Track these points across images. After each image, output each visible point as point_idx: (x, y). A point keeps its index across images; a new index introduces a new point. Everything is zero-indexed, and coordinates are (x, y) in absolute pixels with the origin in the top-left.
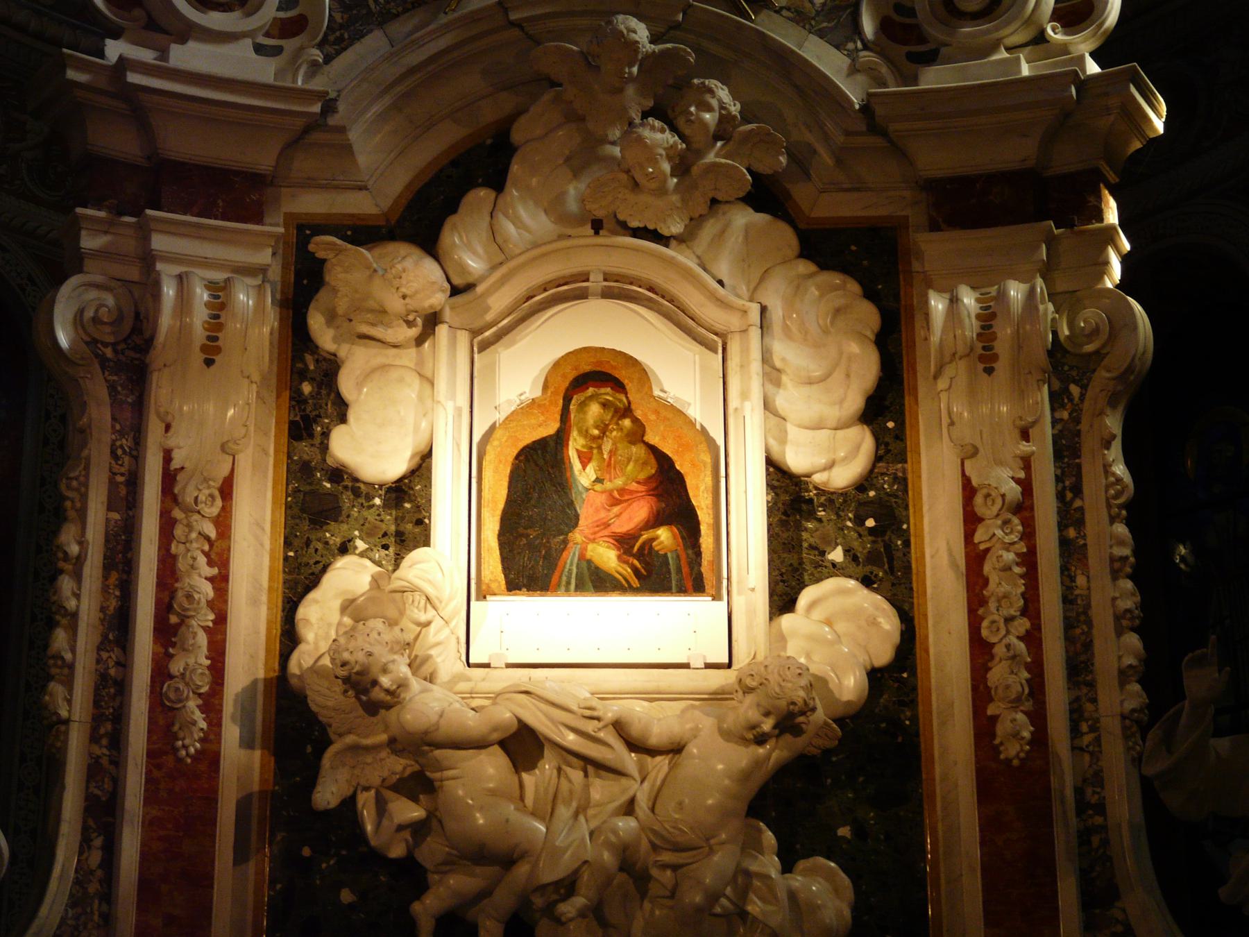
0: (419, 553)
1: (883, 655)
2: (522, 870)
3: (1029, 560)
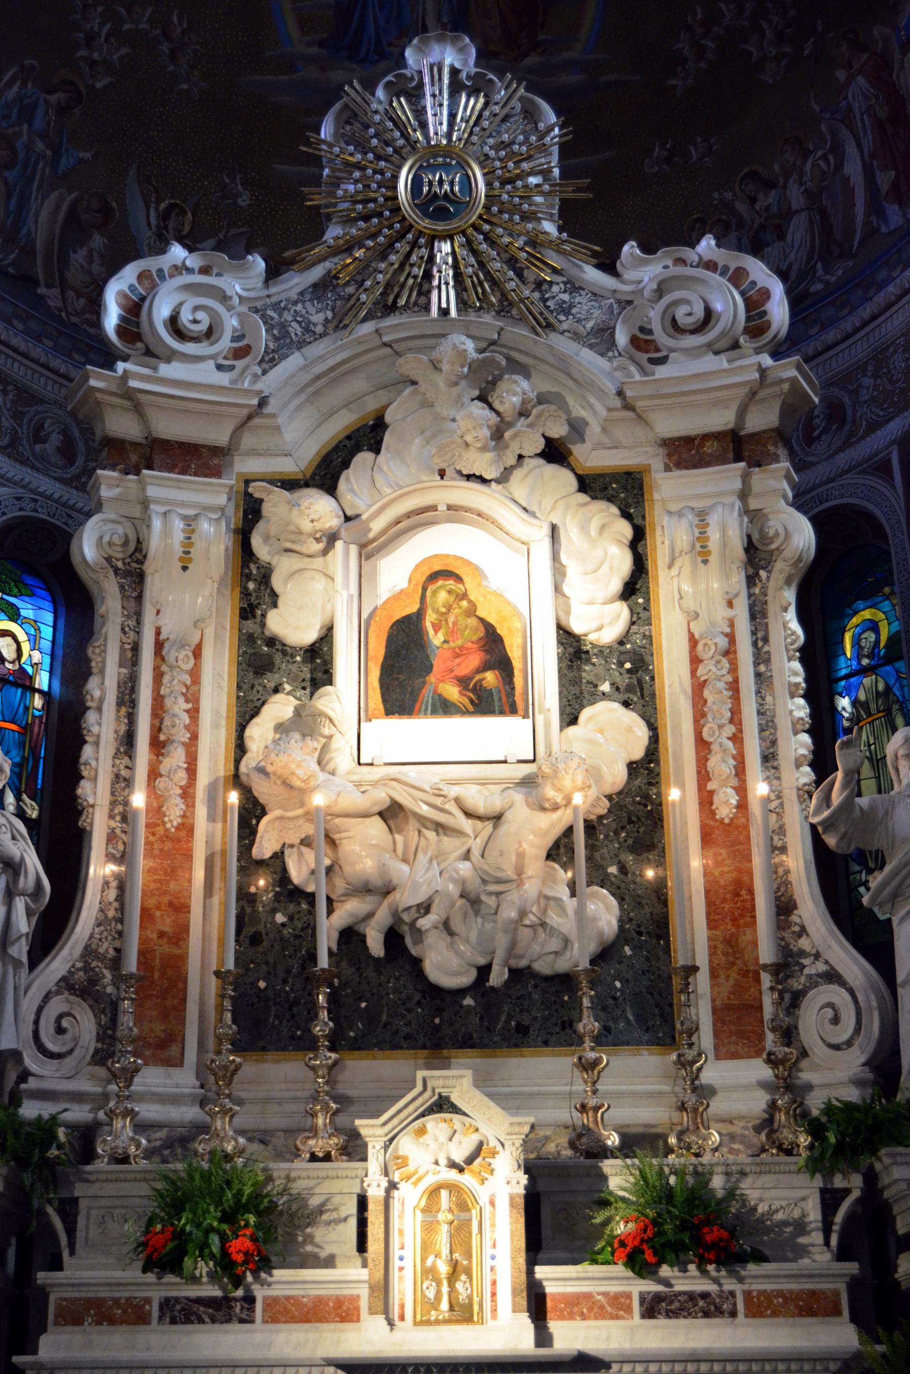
1: (638, 752)
2: (395, 896)
3: (734, 687)
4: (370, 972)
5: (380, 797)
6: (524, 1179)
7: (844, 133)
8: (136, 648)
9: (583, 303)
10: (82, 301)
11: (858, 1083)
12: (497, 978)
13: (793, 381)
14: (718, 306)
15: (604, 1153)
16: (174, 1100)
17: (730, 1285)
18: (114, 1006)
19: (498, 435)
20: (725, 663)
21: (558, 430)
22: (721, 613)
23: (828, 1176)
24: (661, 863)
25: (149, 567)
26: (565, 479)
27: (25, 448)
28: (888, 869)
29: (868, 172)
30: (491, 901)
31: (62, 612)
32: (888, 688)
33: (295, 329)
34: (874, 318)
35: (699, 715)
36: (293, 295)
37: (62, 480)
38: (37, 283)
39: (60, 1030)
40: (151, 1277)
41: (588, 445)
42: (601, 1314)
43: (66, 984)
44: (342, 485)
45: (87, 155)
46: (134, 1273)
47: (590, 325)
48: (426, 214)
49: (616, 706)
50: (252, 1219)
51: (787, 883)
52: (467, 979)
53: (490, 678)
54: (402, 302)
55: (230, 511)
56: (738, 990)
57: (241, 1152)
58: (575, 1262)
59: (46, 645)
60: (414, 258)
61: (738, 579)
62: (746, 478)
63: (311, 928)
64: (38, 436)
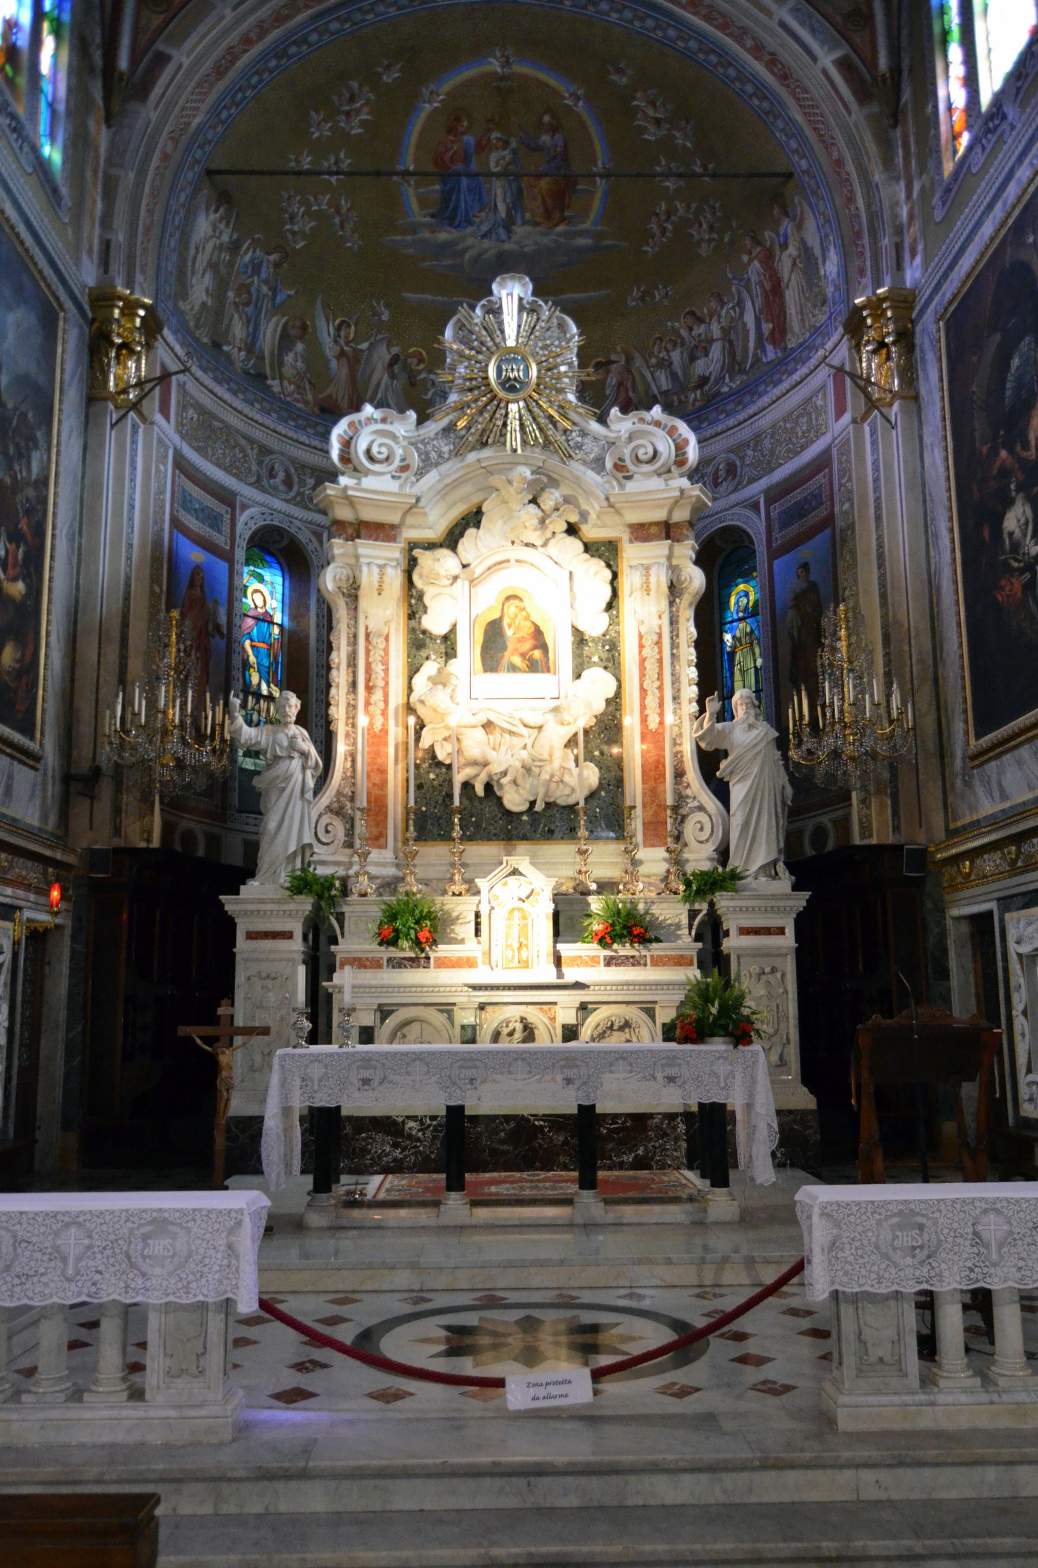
0: (453, 661)
1: (611, 694)
2: (490, 767)
3: (660, 661)
4: (477, 803)
5: (482, 718)
6: (553, 906)
7: (745, 294)
8: (355, 636)
9: (588, 442)
10: (292, 387)
11: (711, 859)
12: (539, 807)
13: (698, 497)
14: (661, 448)
15: (588, 893)
16: (383, 865)
17: (644, 952)
18: (352, 819)
19: (542, 521)
20: (656, 649)
21: (574, 518)
22: (655, 622)
23: (692, 903)
24: (621, 745)
25: (361, 593)
26: (576, 545)
27: (265, 482)
28: (730, 759)
29: (758, 320)
30: (537, 770)
31: (287, 577)
32: (752, 631)
33: (433, 455)
34: (755, 414)
35: (642, 676)
36: (432, 435)
37: (286, 501)
38: (265, 378)
39: (327, 832)
40: (383, 948)
41: (590, 525)
42: (586, 965)
43: (329, 809)
44: (460, 547)
45: (292, 292)
46: (375, 946)
47: (592, 456)
48: (504, 388)
49: (602, 670)
50: (428, 923)
51: (682, 762)
52: (525, 807)
53: (537, 654)
54: (490, 441)
55: (401, 560)
56: (656, 814)
57: (420, 892)
58: (575, 942)
59: (279, 596)
60: (497, 415)
61: (664, 605)
62: (671, 549)
63: (450, 782)
64: (272, 475)
